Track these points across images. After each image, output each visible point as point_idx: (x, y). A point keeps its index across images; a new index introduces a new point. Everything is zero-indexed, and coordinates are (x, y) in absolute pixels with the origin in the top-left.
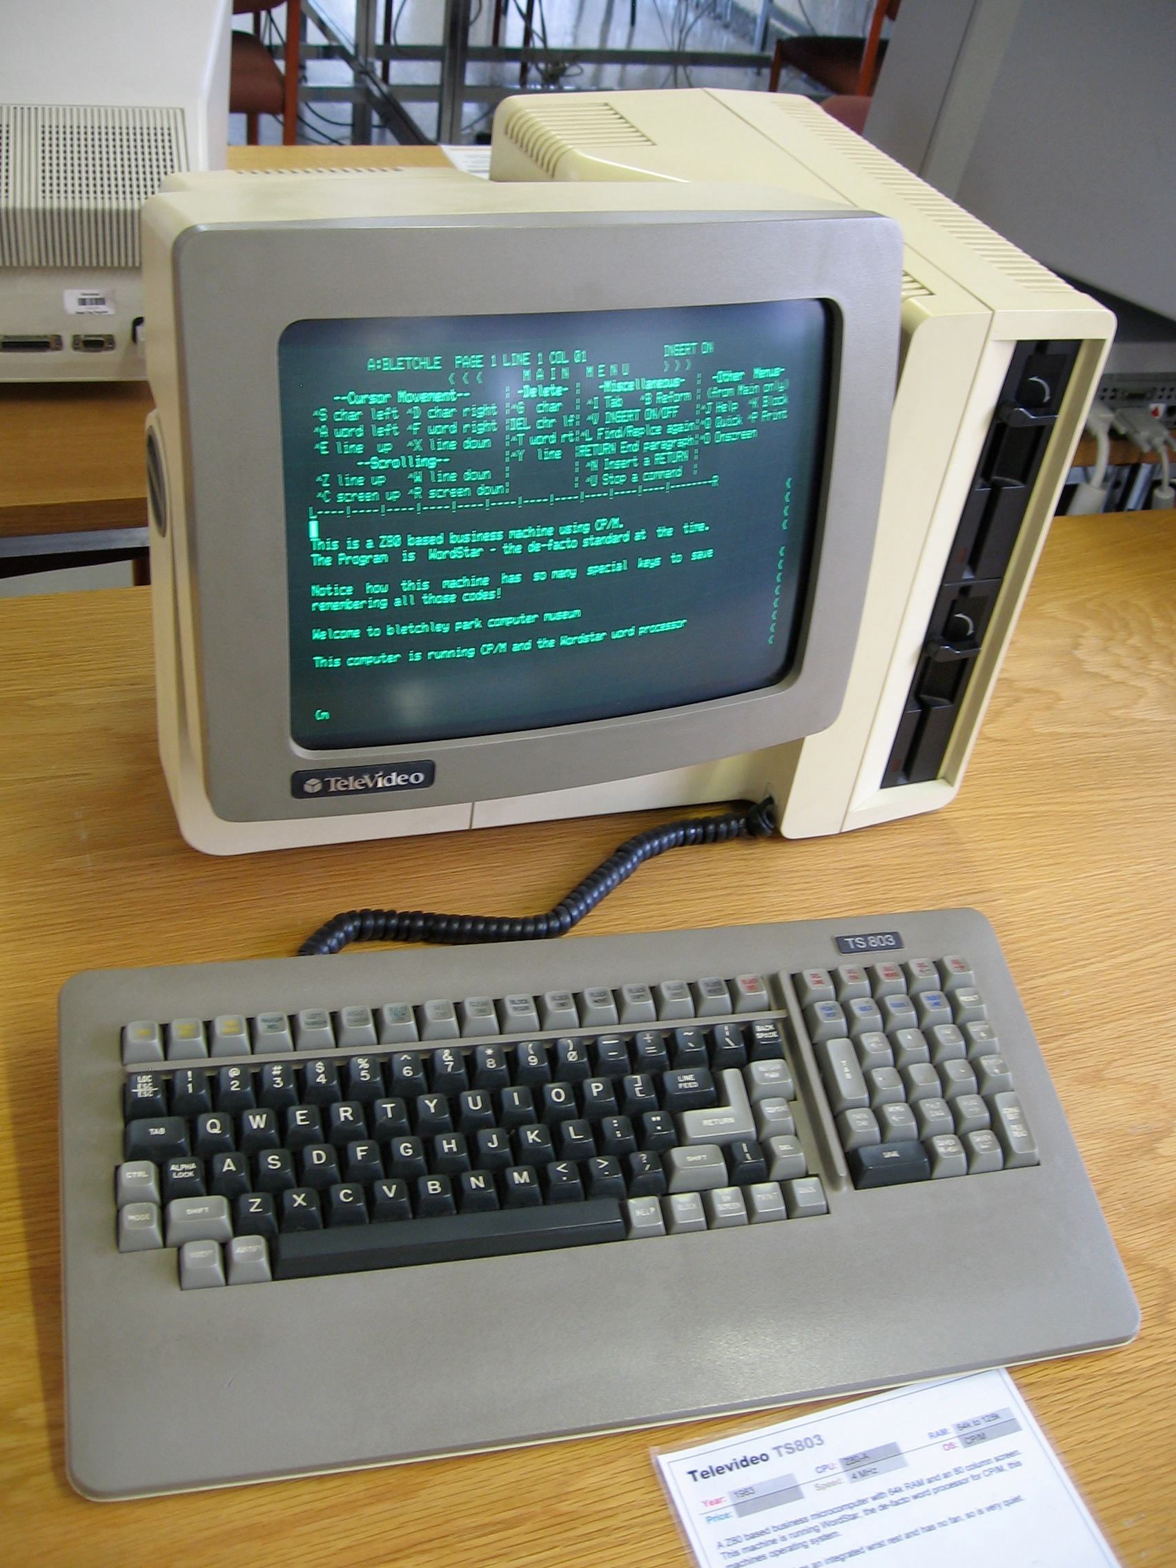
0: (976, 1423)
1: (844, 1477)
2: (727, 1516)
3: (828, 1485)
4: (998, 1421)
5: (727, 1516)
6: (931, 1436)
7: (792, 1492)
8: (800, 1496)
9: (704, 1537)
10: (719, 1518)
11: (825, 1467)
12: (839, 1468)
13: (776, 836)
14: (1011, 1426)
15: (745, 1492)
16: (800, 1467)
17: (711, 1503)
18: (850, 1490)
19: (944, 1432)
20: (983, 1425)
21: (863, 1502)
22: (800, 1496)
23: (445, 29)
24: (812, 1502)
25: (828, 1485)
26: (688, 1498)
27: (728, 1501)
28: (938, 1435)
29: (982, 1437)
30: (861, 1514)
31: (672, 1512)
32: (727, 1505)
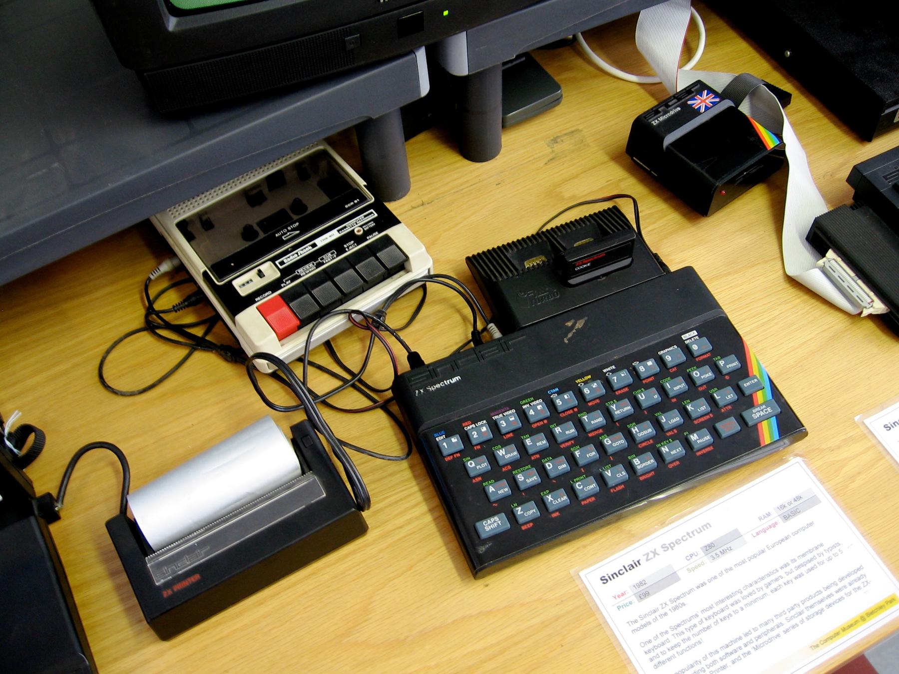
0: (790, 503)
1: (705, 559)
2: (631, 603)
3: (696, 567)
4: (801, 501)
5: (631, 603)
6: (760, 519)
7: (672, 578)
8: (678, 579)
9: (632, 644)
10: (626, 605)
11: (691, 556)
12: (702, 553)
13: (482, 343)
14: (814, 501)
15: (641, 584)
16: (675, 559)
17: (619, 596)
18: (712, 567)
19: (769, 514)
20: (795, 504)
21: (786, 631)
22: (678, 579)
23: (541, 552)
24: (687, 581)
25: (696, 567)
26: (604, 597)
27: (775, 514)
28: (765, 517)
29: (795, 512)
30: (782, 634)
31: (580, 587)
32: (631, 596)
